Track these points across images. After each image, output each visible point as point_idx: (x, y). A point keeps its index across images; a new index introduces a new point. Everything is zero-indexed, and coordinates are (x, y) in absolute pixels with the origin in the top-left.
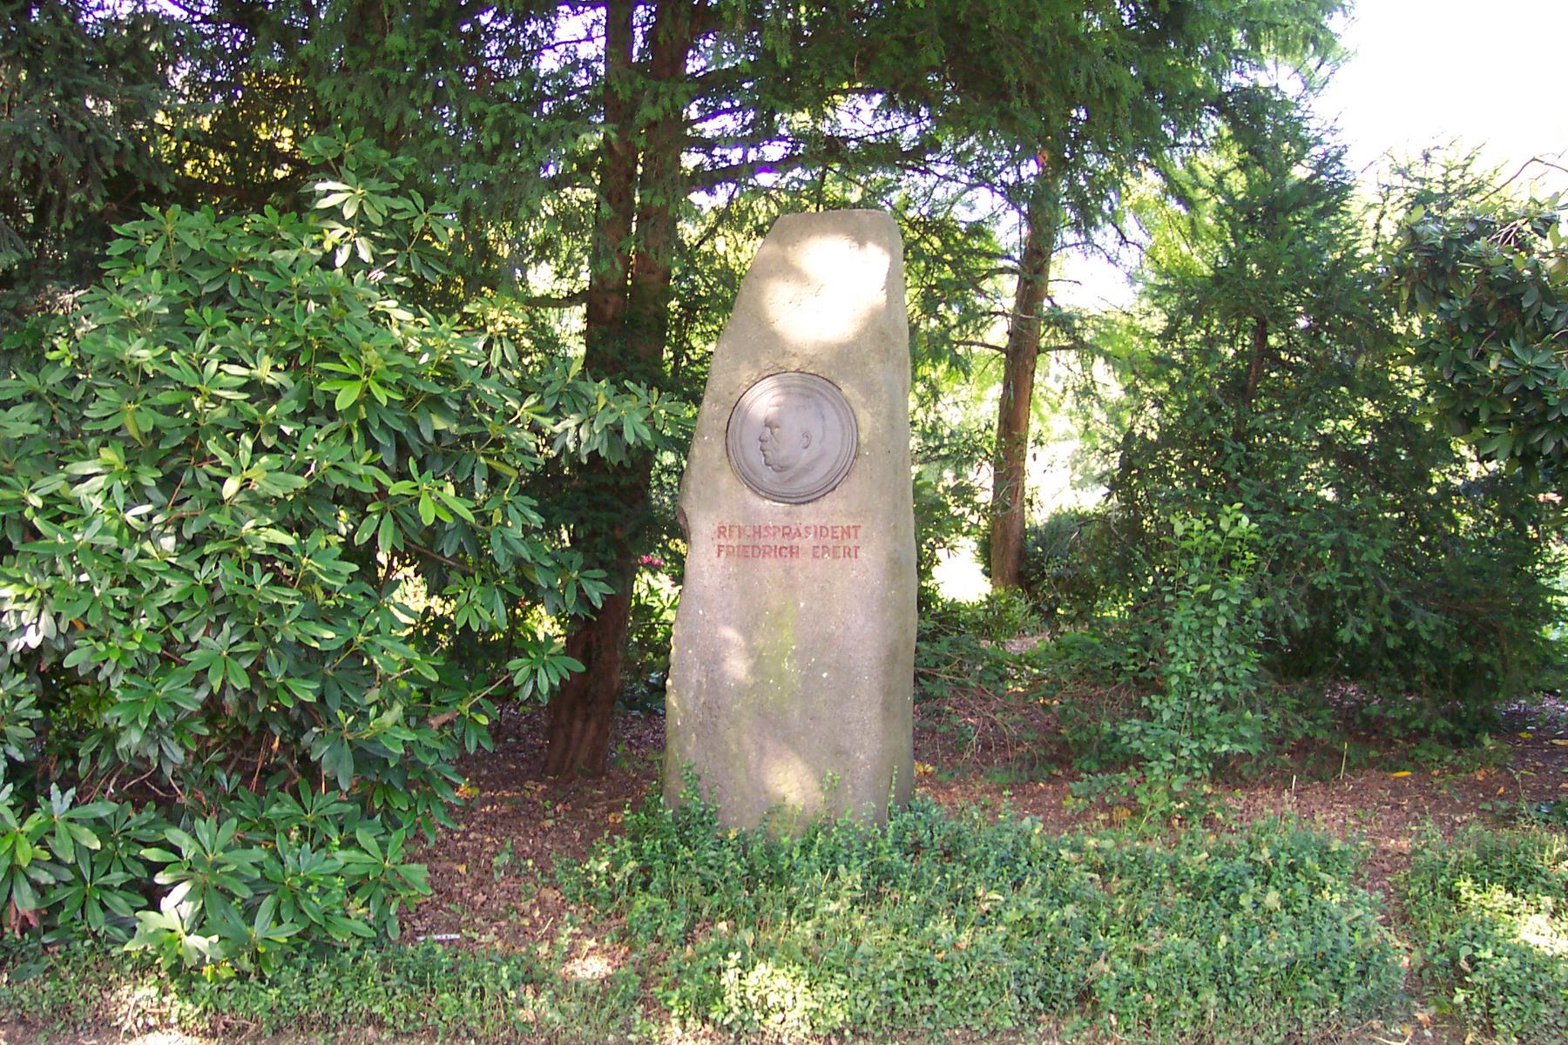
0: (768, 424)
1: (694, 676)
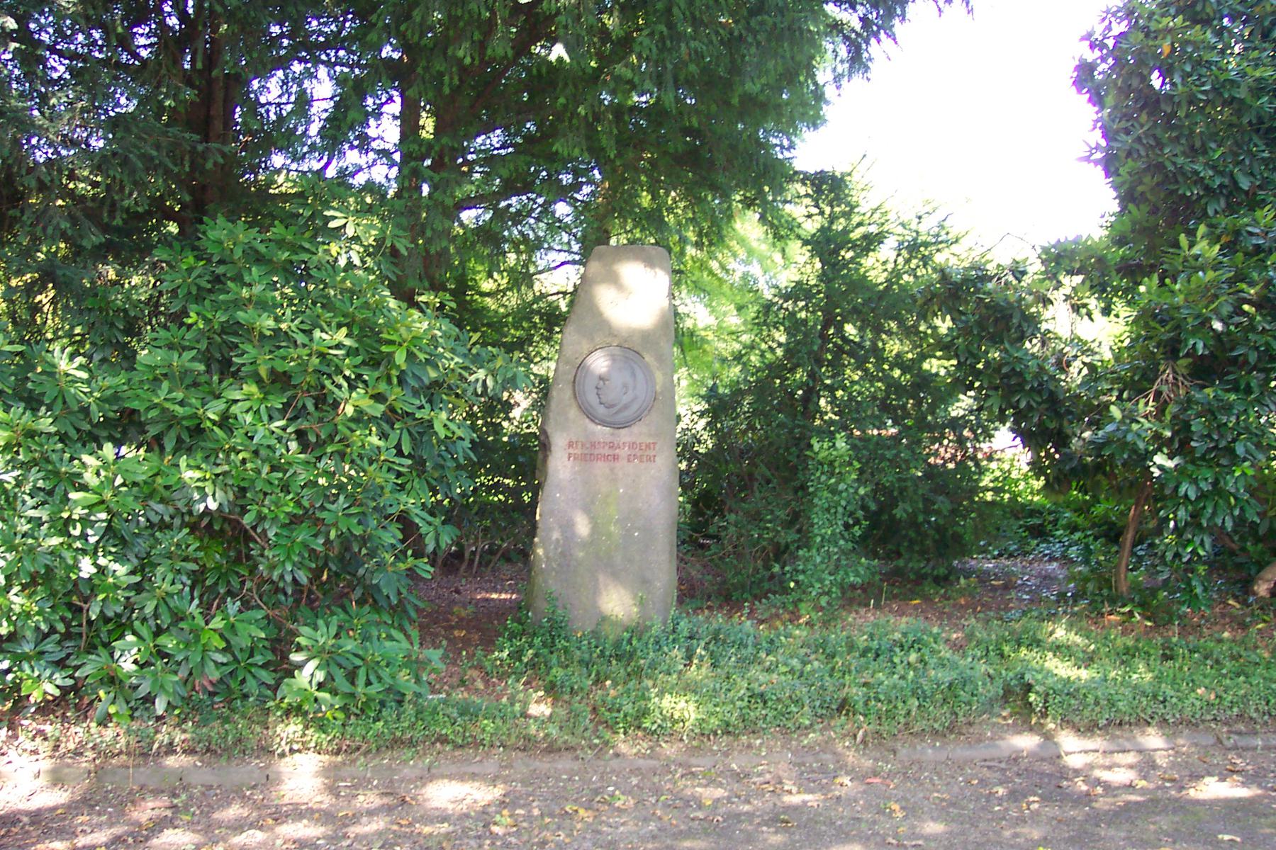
0: (601, 378)
1: (556, 535)
